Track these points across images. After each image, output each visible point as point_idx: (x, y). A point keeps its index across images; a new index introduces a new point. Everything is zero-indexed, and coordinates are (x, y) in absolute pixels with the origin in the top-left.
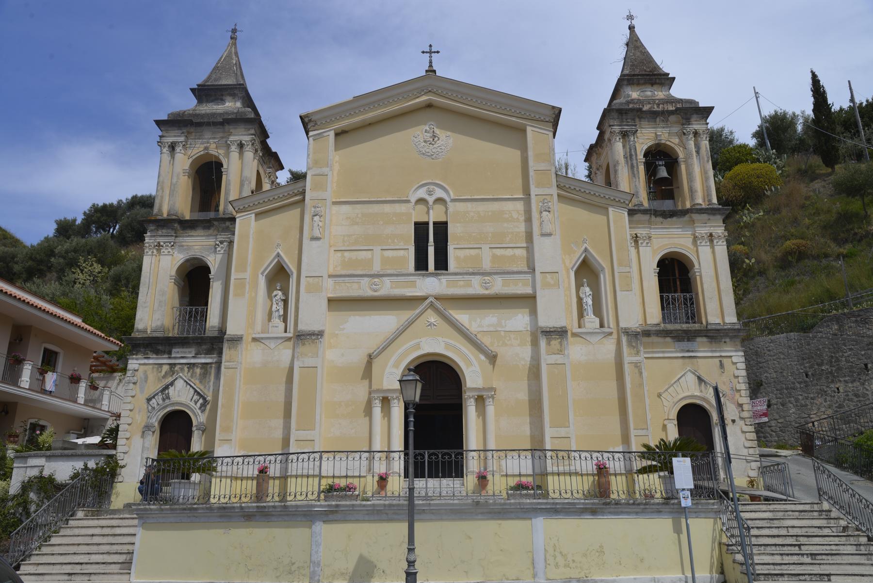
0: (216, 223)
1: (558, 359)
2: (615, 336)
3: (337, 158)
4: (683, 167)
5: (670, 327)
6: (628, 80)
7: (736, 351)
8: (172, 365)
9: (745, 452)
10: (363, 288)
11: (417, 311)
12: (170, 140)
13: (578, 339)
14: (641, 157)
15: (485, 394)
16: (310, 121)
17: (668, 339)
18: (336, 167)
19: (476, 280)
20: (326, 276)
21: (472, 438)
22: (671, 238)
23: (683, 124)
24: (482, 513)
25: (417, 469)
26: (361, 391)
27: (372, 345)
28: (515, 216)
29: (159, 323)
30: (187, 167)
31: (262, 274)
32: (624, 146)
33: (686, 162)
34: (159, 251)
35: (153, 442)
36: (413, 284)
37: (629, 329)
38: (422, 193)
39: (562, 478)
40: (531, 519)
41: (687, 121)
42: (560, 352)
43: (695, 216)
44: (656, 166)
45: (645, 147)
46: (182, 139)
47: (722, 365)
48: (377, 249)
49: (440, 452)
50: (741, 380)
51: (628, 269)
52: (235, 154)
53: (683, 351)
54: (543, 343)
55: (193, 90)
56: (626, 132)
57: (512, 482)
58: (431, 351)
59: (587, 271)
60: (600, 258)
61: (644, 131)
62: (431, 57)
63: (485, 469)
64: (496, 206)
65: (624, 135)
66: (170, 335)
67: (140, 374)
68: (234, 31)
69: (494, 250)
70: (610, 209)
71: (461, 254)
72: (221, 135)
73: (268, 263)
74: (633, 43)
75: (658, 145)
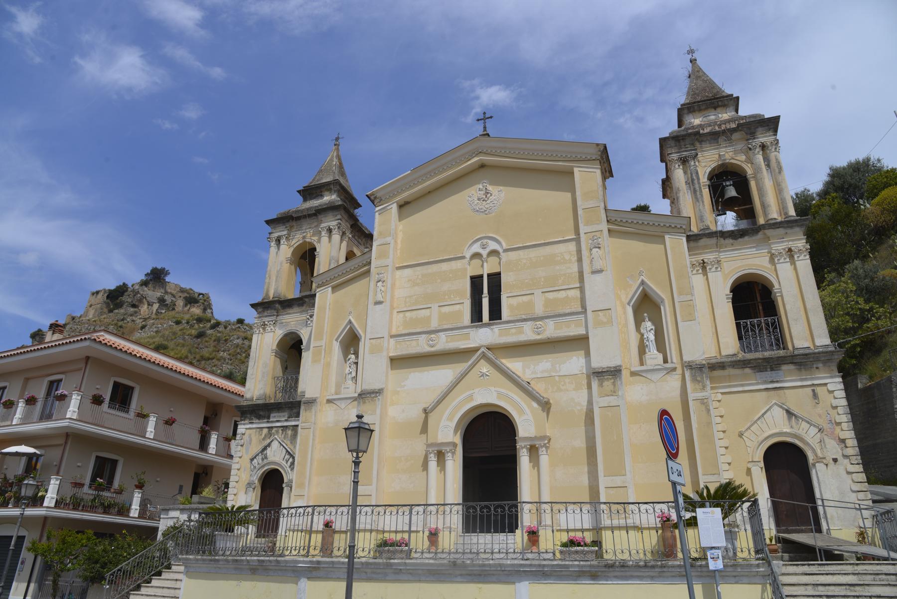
0: (307, 300)
1: (612, 401)
2: (679, 371)
3: (401, 227)
4: (753, 184)
5: (749, 356)
6: (689, 109)
7: (832, 377)
8: (270, 428)
9: (853, 497)
10: (421, 345)
11: (470, 362)
12: (276, 235)
13: (638, 378)
14: (704, 179)
15: (537, 443)
16: (375, 198)
17: (747, 370)
18: (400, 236)
19: (528, 327)
20: (386, 335)
21: (526, 489)
22: (748, 260)
23: (748, 140)
24: (461, 575)
25: (475, 522)
26: (419, 447)
27: (428, 400)
28: (567, 257)
29: (262, 392)
30: (289, 255)
31: (337, 340)
32: (685, 173)
33: (755, 177)
34: (264, 329)
35: (254, 498)
36: (467, 337)
37: (693, 362)
38: (476, 248)
39: (616, 532)
40: (514, 583)
41: (752, 135)
42: (614, 393)
43: (769, 232)
44: (724, 187)
45: (709, 169)
46: (285, 233)
47: (815, 395)
48: (435, 306)
49: (492, 504)
50: (840, 410)
51: (689, 297)
52: (325, 239)
53: (765, 382)
54: (595, 384)
55: (299, 192)
56: (686, 157)
57: (565, 538)
58: (484, 401)
59: (646, 305)
60: (658, 290)
61: (706, 154)
62: (485, 123)
63: (540, 522)
64: (548, 250)
65: (684, 161)
66: (272, 401)
67: (246, 437)
68: (337, 139)
69: (546, 294)
70: (667, 237)
71: (514, 301)
72: (316, 224)
73: (341, 328)
74: (696, 74)
75: (723, 165)
